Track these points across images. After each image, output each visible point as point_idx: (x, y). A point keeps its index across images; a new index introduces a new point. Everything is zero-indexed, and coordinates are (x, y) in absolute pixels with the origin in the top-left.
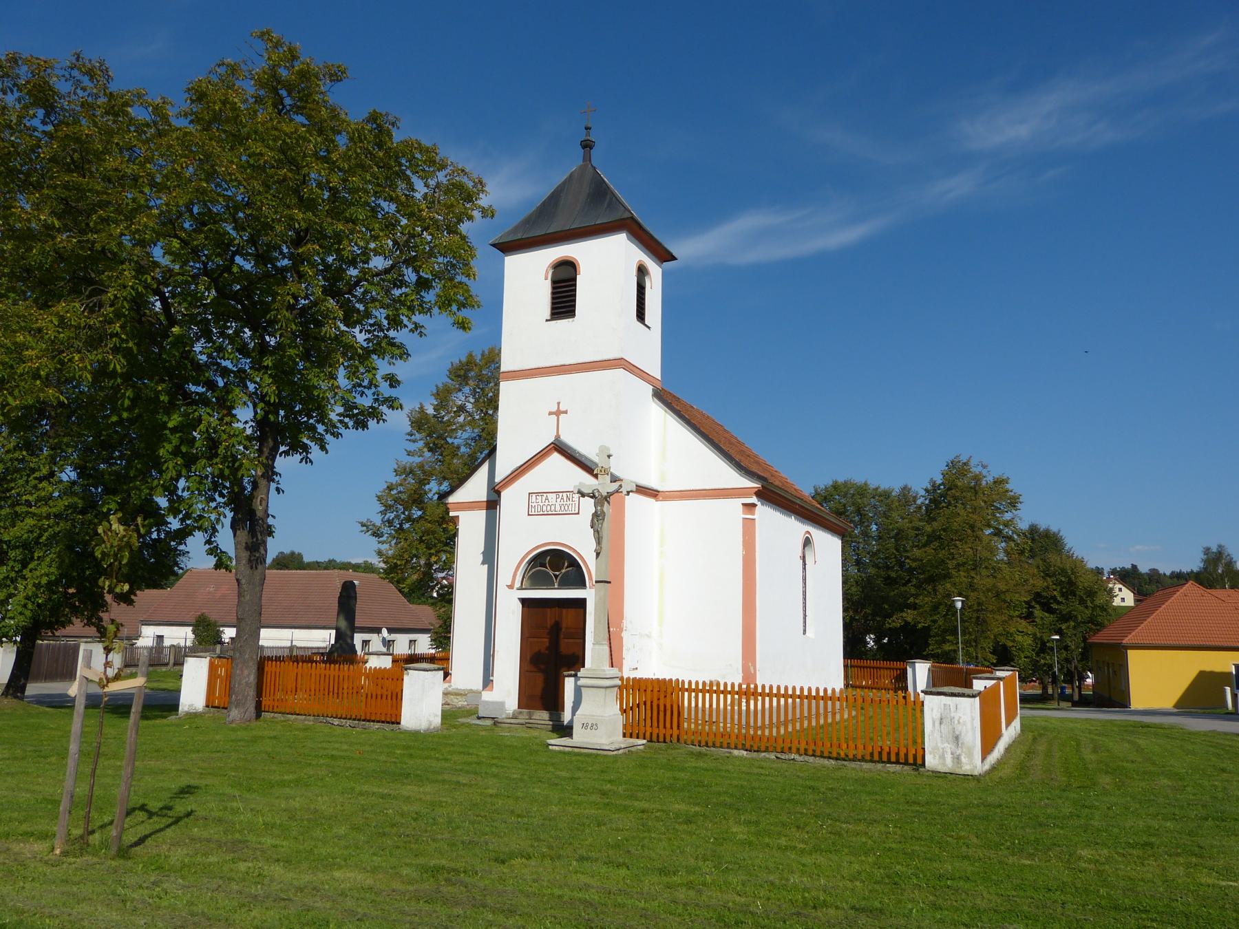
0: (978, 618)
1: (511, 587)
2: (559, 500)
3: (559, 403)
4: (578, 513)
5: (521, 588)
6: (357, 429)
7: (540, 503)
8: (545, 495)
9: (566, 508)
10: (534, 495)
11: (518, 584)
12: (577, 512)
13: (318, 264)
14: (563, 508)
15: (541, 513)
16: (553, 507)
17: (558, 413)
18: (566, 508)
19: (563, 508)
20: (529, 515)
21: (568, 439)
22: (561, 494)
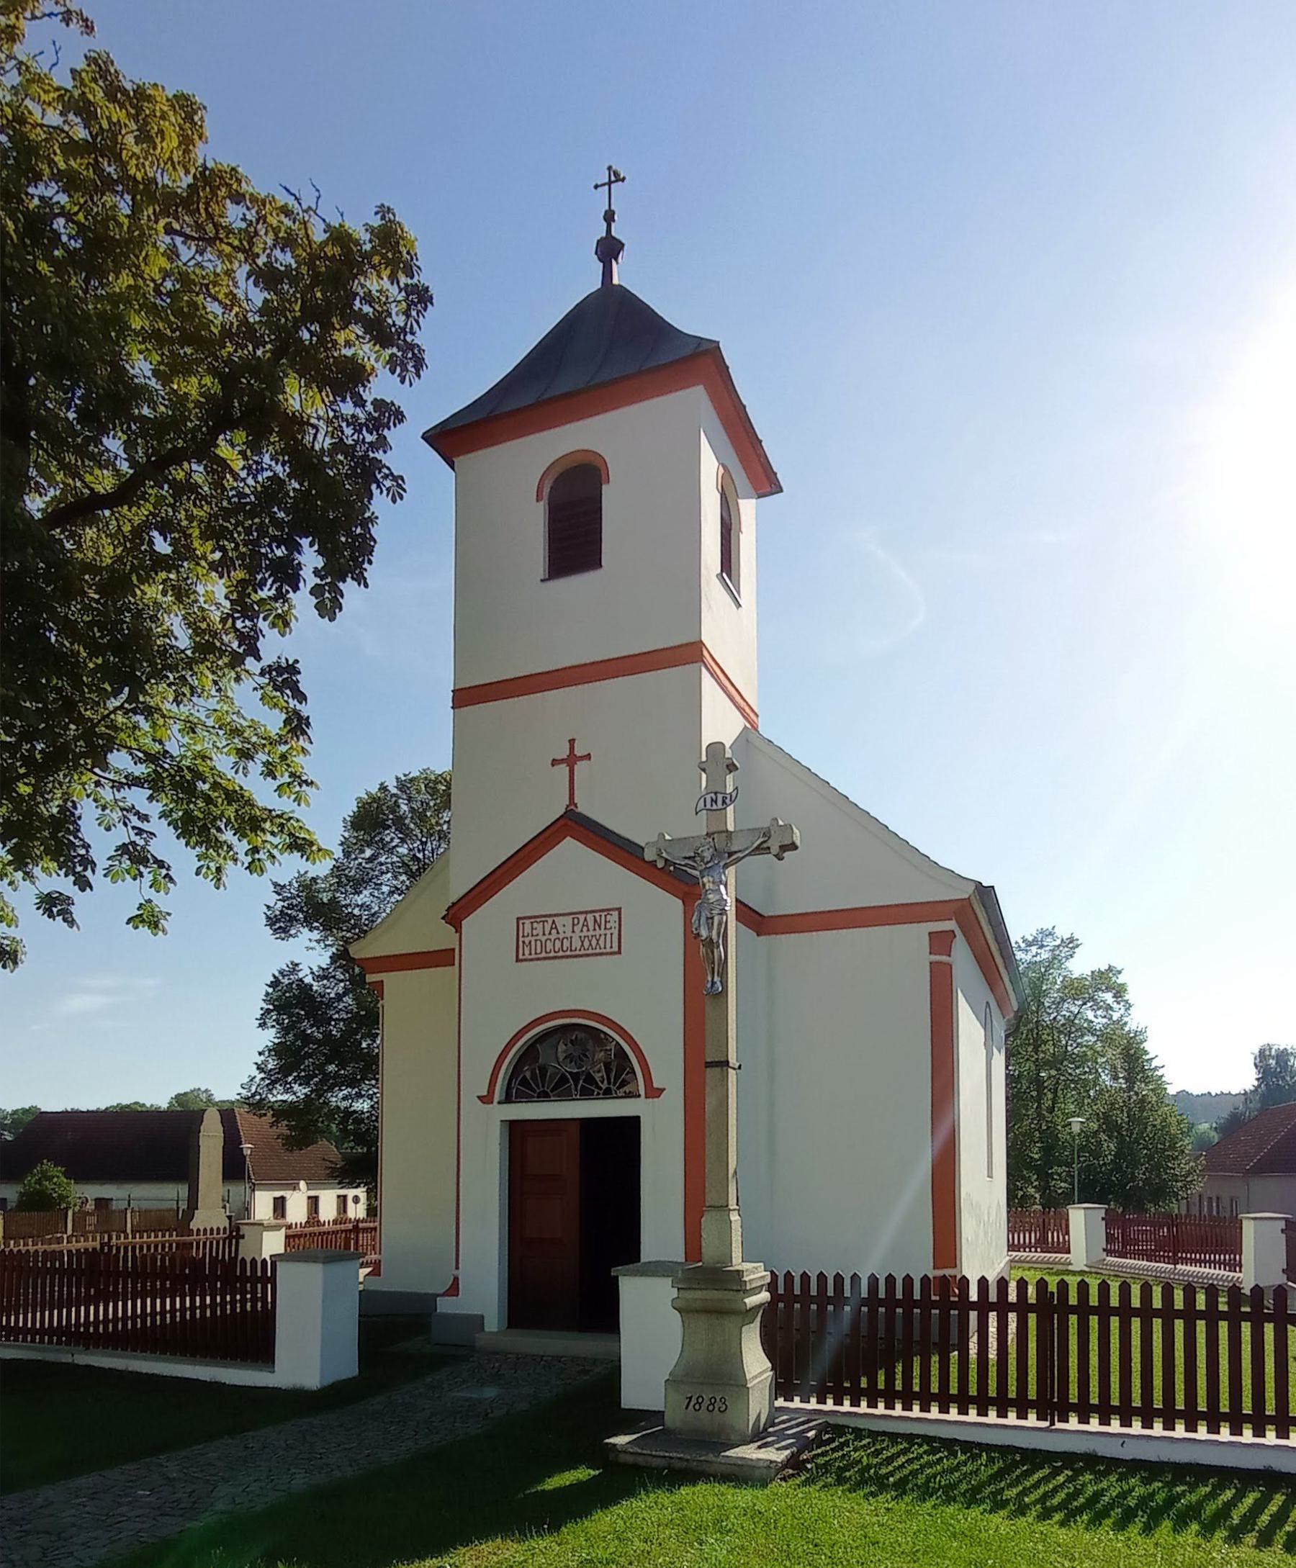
0: (103, 810)
1: (486, 1099)
2: (577, 929)
3: (572, 742)
4: (518, 919)
5: (508, 1099)
6: (342, 844)
7: (540, 937)
8: (550, 920)
9: (594, 942)
10: (527, 922)
11: (498, 1093)
12: (521, 922)
13: (145, 336)
14: (586, 944)
15: (544, 955)
16: (566, 943)
17: (571, 760)
18: (594, 942)
19: (586, 944)
20: (518, 960)
21: (585, 807)
22: (582, 917)
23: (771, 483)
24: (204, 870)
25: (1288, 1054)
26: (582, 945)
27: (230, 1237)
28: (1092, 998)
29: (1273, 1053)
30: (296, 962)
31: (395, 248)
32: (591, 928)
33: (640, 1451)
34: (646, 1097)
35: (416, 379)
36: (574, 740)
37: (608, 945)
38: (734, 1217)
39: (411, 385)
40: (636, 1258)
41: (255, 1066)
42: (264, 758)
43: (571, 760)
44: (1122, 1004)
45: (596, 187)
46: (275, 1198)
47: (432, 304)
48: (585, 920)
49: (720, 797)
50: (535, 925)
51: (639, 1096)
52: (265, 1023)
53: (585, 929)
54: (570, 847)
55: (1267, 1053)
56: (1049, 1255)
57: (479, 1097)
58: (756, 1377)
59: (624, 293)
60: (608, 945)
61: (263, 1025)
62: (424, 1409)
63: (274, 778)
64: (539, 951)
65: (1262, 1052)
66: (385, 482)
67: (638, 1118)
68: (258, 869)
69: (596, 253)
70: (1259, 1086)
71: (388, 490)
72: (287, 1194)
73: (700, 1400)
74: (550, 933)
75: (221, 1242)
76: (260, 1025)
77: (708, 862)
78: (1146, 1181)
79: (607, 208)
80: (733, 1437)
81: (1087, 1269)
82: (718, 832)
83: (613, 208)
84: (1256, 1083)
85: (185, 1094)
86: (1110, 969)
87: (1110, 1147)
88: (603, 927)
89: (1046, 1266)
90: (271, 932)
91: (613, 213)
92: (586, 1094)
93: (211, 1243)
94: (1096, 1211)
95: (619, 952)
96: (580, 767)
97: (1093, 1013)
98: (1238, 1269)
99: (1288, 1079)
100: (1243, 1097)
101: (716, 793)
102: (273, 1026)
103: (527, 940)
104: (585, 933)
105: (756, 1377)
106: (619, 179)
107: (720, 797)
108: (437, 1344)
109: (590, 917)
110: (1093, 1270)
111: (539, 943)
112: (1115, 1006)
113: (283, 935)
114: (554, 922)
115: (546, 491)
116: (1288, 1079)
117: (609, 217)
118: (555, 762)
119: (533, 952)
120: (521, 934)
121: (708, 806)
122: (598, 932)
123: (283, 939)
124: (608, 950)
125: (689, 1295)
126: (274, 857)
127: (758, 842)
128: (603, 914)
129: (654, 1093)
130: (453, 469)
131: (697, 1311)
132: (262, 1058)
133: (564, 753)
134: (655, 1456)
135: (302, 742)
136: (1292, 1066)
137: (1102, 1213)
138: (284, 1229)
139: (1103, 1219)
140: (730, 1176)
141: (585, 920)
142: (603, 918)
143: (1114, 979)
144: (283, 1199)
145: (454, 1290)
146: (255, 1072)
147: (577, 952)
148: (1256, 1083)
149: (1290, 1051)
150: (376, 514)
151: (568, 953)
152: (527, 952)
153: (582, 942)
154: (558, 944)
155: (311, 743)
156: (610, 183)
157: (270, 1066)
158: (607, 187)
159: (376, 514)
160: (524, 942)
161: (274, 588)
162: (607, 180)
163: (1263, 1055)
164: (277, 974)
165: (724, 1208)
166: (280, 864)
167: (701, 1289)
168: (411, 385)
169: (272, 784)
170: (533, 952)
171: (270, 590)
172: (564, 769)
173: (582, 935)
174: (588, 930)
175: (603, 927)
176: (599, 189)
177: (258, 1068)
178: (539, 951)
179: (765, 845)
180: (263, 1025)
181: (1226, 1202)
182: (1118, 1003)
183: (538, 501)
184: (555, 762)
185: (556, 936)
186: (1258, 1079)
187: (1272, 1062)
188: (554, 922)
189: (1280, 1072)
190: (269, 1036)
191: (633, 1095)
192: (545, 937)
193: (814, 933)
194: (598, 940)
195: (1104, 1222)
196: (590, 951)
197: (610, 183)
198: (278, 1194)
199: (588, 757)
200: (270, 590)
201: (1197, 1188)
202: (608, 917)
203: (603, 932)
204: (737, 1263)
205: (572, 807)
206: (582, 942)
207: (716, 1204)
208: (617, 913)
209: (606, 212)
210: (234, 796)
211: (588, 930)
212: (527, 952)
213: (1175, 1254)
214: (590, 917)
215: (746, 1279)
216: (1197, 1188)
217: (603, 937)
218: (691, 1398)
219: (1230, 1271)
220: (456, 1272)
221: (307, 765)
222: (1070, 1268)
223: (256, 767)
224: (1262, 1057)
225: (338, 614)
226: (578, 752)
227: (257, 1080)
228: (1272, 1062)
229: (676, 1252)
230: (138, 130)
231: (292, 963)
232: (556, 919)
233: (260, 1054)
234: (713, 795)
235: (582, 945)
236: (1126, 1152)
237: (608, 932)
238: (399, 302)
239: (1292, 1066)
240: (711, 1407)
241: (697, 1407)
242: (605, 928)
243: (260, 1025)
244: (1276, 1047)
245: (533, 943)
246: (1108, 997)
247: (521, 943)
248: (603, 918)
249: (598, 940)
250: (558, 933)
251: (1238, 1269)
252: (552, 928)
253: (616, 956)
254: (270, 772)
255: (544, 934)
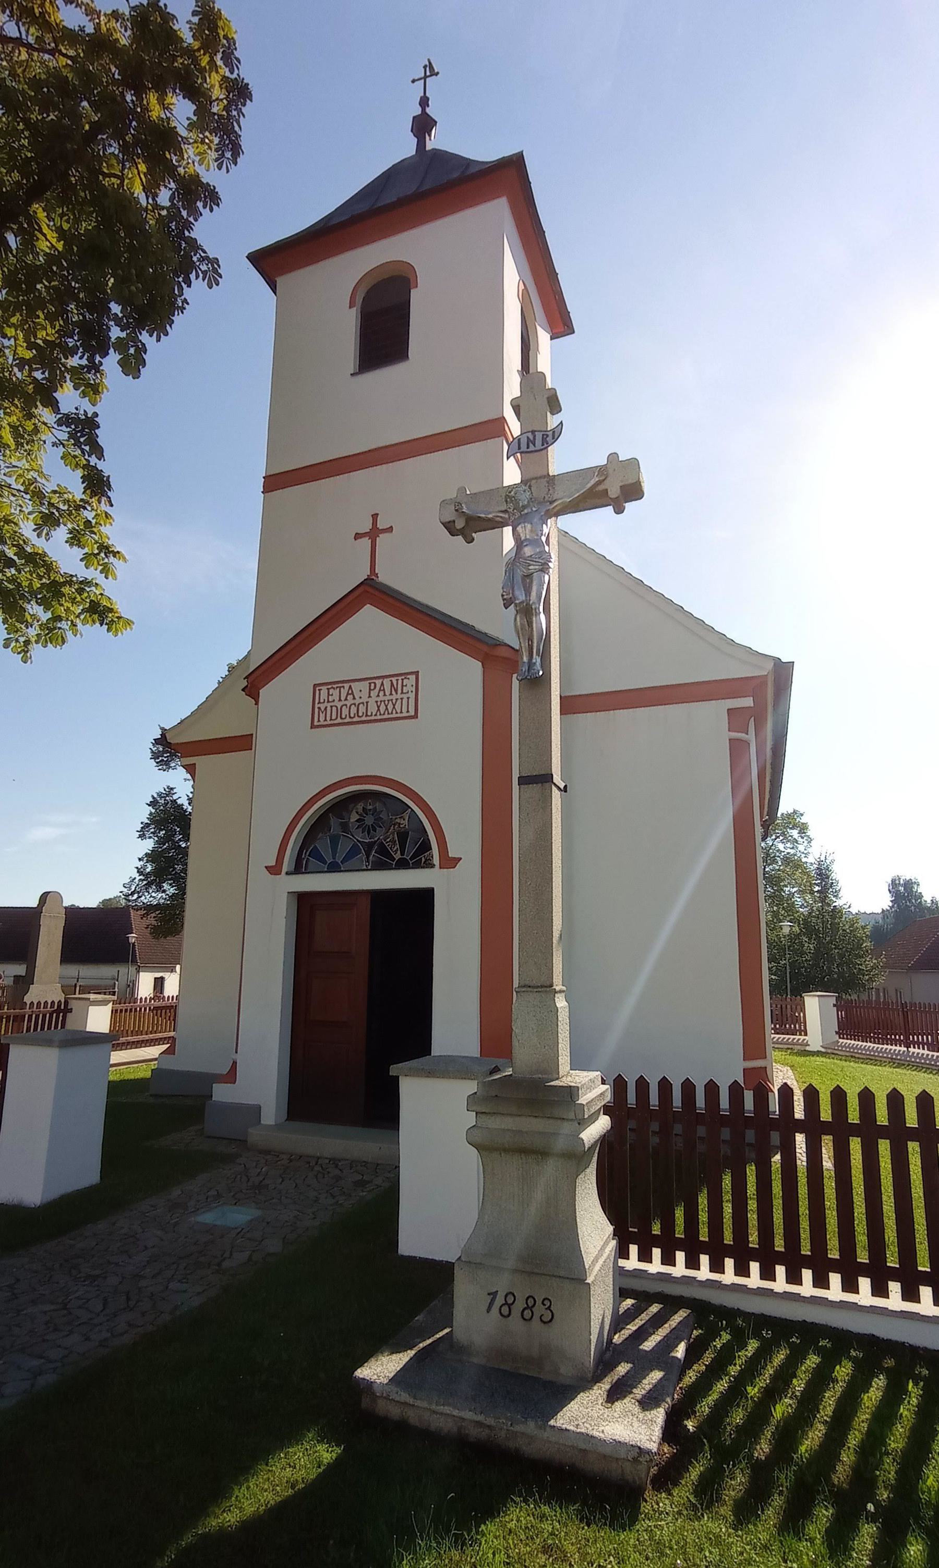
1: (274, 870)
2: (374, 694)
3: (375, 517)
5: (299, 868)
8: (347, 686)
9: (390, 707)
10: (324, 688)
15: (339, 720)
16: (362, 709)
17: (374, 533)
18: (390, 707)
20: (313, 726)
21: (384, 577)
22: (378, 682)
23: (565, 324)
24: (13, 644)
25: (912, 883)
26: (379, 710)
27: (58, 1011)
28: (783, 834)
29: (902, 882)
30: (171, 786)
31: (214, 28)
32: (387, 693)
33: (411, 1401)
34: (440, 868)
35: (233, 166)
36: (377, 514)
37: (404, 710)
38: (561, 1003)
39: (228, 171)
40: (425, 1048)
41: (136, 870)
42: (70, 526)
43: (374, 533)
44: (805, 838)
45: (413, 81)
46: (155, 978)
47: (251, 100)
48: (382, 684)
49: (539, 436)
50: (331, 691)
51: (433, 866)
52: (144, 835)
53: (382, 693)
54: (369, 614)
55: (897, 882)
56: (783, 1036)
57: (266, 867)
58: (596, 1260)
59: (437, 153)
60: (404, 710)
61: (142, 836)
62: (146, 1248)
63: (80, 545)
64: (334, 717)
65: (893, 881)
66: (201, 267)
67: (433, 889)
68: (60, 639)
69: (412, 131)
70: (893, 906)
71: (205, 273)
72: (166, 975)
73: (510, 1300)
74: (346, 699)
75: (48, 1015)
76: (140, 836)
77: (524, 507)
78: (839, 973)
79: (422, 94)
80: (563, 1370)
81: (823, 1050)
82: (536, 478)
83: (427, 95)
84: (891, 904)
85: (110, 899)
86: (795, 812)
87: (810, 946)
88: (399, 691)
89: (786, 1046)
90: (155, 764)
91: (428, 99)
92: (380, 866)
93: (44, 1016)
94: (830, 998)
95: (415, 716)
96: (381, 540)
97: (783, 845)
98: (803, 1033)
99: (914, 901)
100: (881, 916)
101: (533, 432)
102: (150, 838)
103: (323, 707)
104: (382, 698)
105: (596, 1260)
106: (434, 73)
107: (539, 436)
108: (209, 1137)
109: (387, 683)
110: (829, 1051)
111: (334, 709)
112: (800, 840)
113: (165, 767)
114: (350, 687)
115: (359, 300)
116: (914, 901)
117: (424, 102)
118: (358, 536)
119: (328, 718)
120: (317, 701)
121: (524, 448)
122: (394, 697)
123: (164, 770)
124: (405, 714)
125: (495, 1123)
126: (75, 626)
127: (592, 482)
128: (400, 678)
129: (450, 862)
130: (275, 293)
131: (506, 1150)
132: (142, 863)
133: (367, 527)
134: (434, 1412)
135: (104, 507)
136: (916, 892)
137: (833, 1001)
138: (111, 1004)
139: (834, 1005)
140: (555, 941)
141: (382, 684)
142: (400, 682)
143: (798, 819)
144: (162, 979)
145: (231, 1076)
146: (136, 875)
147: (373, 718)
148: (891, 904)
149: (913, 881)
150: (82, 26)
151: (364, 718)
152: (322, 719)
153: (378, 707)
154: (353, 709)
155: (112, 505)
156: (425, 77)
157: (148, 870)
158: (423, 81)
159: (82, 26)
160: (319, 708)
161: (86, 357)
162: (423, 75)
163: (894, 884)
164: (155, 796)
165: (547, 988)
166: (82, 636)
167: (511, 1115)
168: (228, 171)
169: (78, 553)
170: (328, 718)
171: (81, 358)
172: (366, 542)
173: (379, 699)
174: (385, 695)
175: (399, 691)
176: (416, 83)
177: (138, 872)
178: (334, 717)
179: (601, 488)
180: (142, 836)
181: (892, 993)
182: (802, 838)
183: (350, 307)
184: (358, 536)
185: (353, 702)
186: (892, 901)
187: (902, 889)
188: (350, 687)
189: (908, 896)
190: (148, 845)
191: (429, 865)
192: (342, 703)
193: (612, 712)
194: (394, 705)
195: (835, 1008)
196: (386, 716)
197: (425, 77)
198: (158, 975)
199: (390, 529)
200: (81, 358)
201: (879, 982)
202: (405, 682)
203: (399, 696)
204: (569, 1076)
205: (373, 577)
206: (378, 707)
207: (534, 983)
208: (414, 676)
209: (421, 98)
210: (37, 560)
211: (385, 695)
212: (322, 719)
213: (907, 1038)
214: (387, 683)
215: (583, 1100)
216: (879, 982)
217: (399, 701)
218: (494, 1295)
219: (863, 1041)
220: (234, 1056)
221: (111, 533)
222: (808, 1048)
223: (61, 533)
224: (894, 884)
225: (142, 370)
226: (380, 526)
227: (136, 880)
228: (902, 889)
229: (471, 1046)
230: (40, 78)
231: (168, 787)
232: (352, 684)
233: (140, 859)
234: (530, 435)
235: (379, 710)
236: (821, 953)
237: (405, 696)
238: (222, 100)
239: (916, 892)
240: (527, 1314)
241: (505, 1310)
242: (402, 693)
243: (140, 836)
244: (904, 878)
245: (329, 709)
246: (795, 833)
247: (316, 710)
248: (400, 682)
249: (394, 705)
250: (354, 698)
251: (803, 1033)
252: (348, 694)
253: (413, 720)
254: (75, 539)
255: (340, 700)
